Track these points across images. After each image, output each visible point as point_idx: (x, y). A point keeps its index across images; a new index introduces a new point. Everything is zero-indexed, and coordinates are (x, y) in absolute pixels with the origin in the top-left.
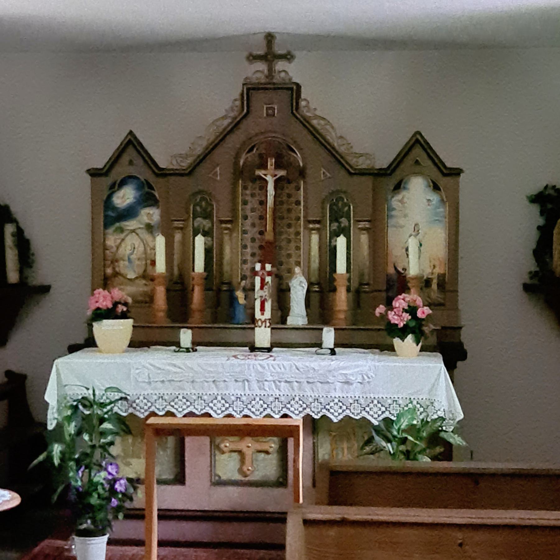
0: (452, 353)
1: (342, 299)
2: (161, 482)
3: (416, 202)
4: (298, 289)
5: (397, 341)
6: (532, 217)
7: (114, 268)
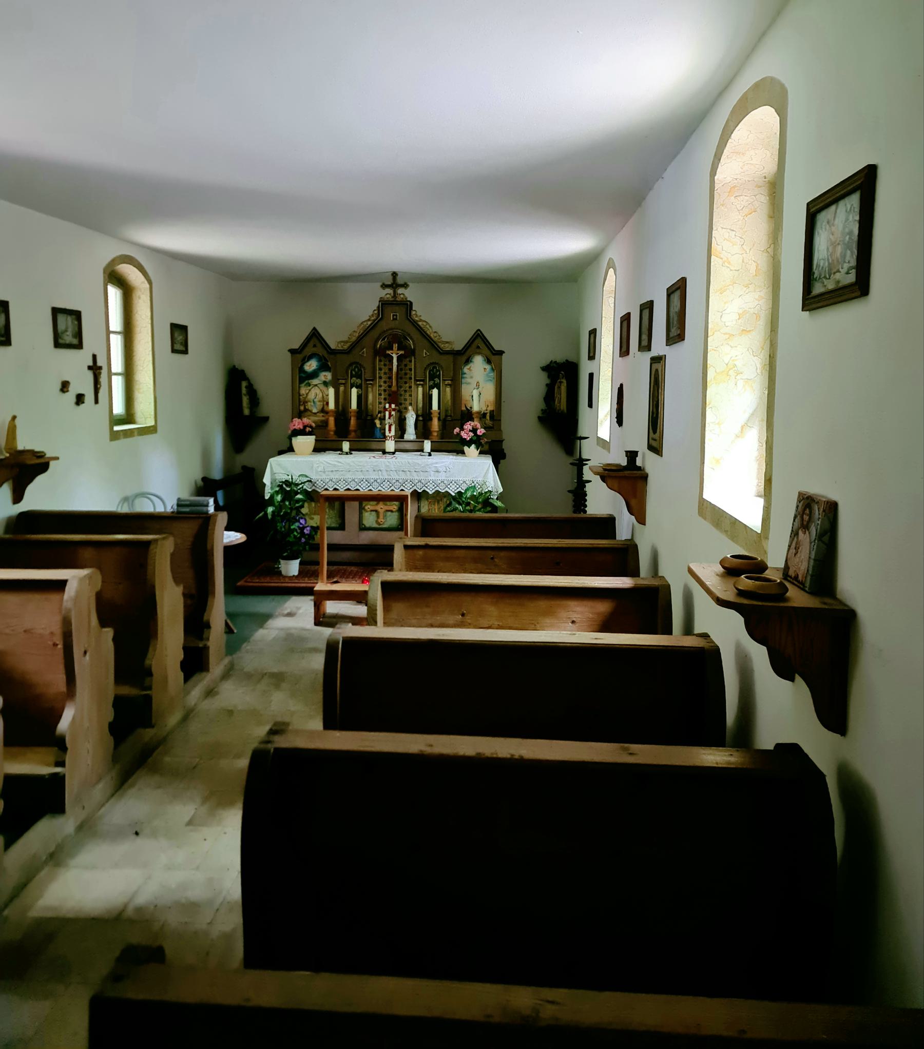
0: (496, 452)
1: (435, 424)
2: (328, 529)
3: (477, 371)
4: (411, 419)
5: (466, 448)
6: (542, 380)
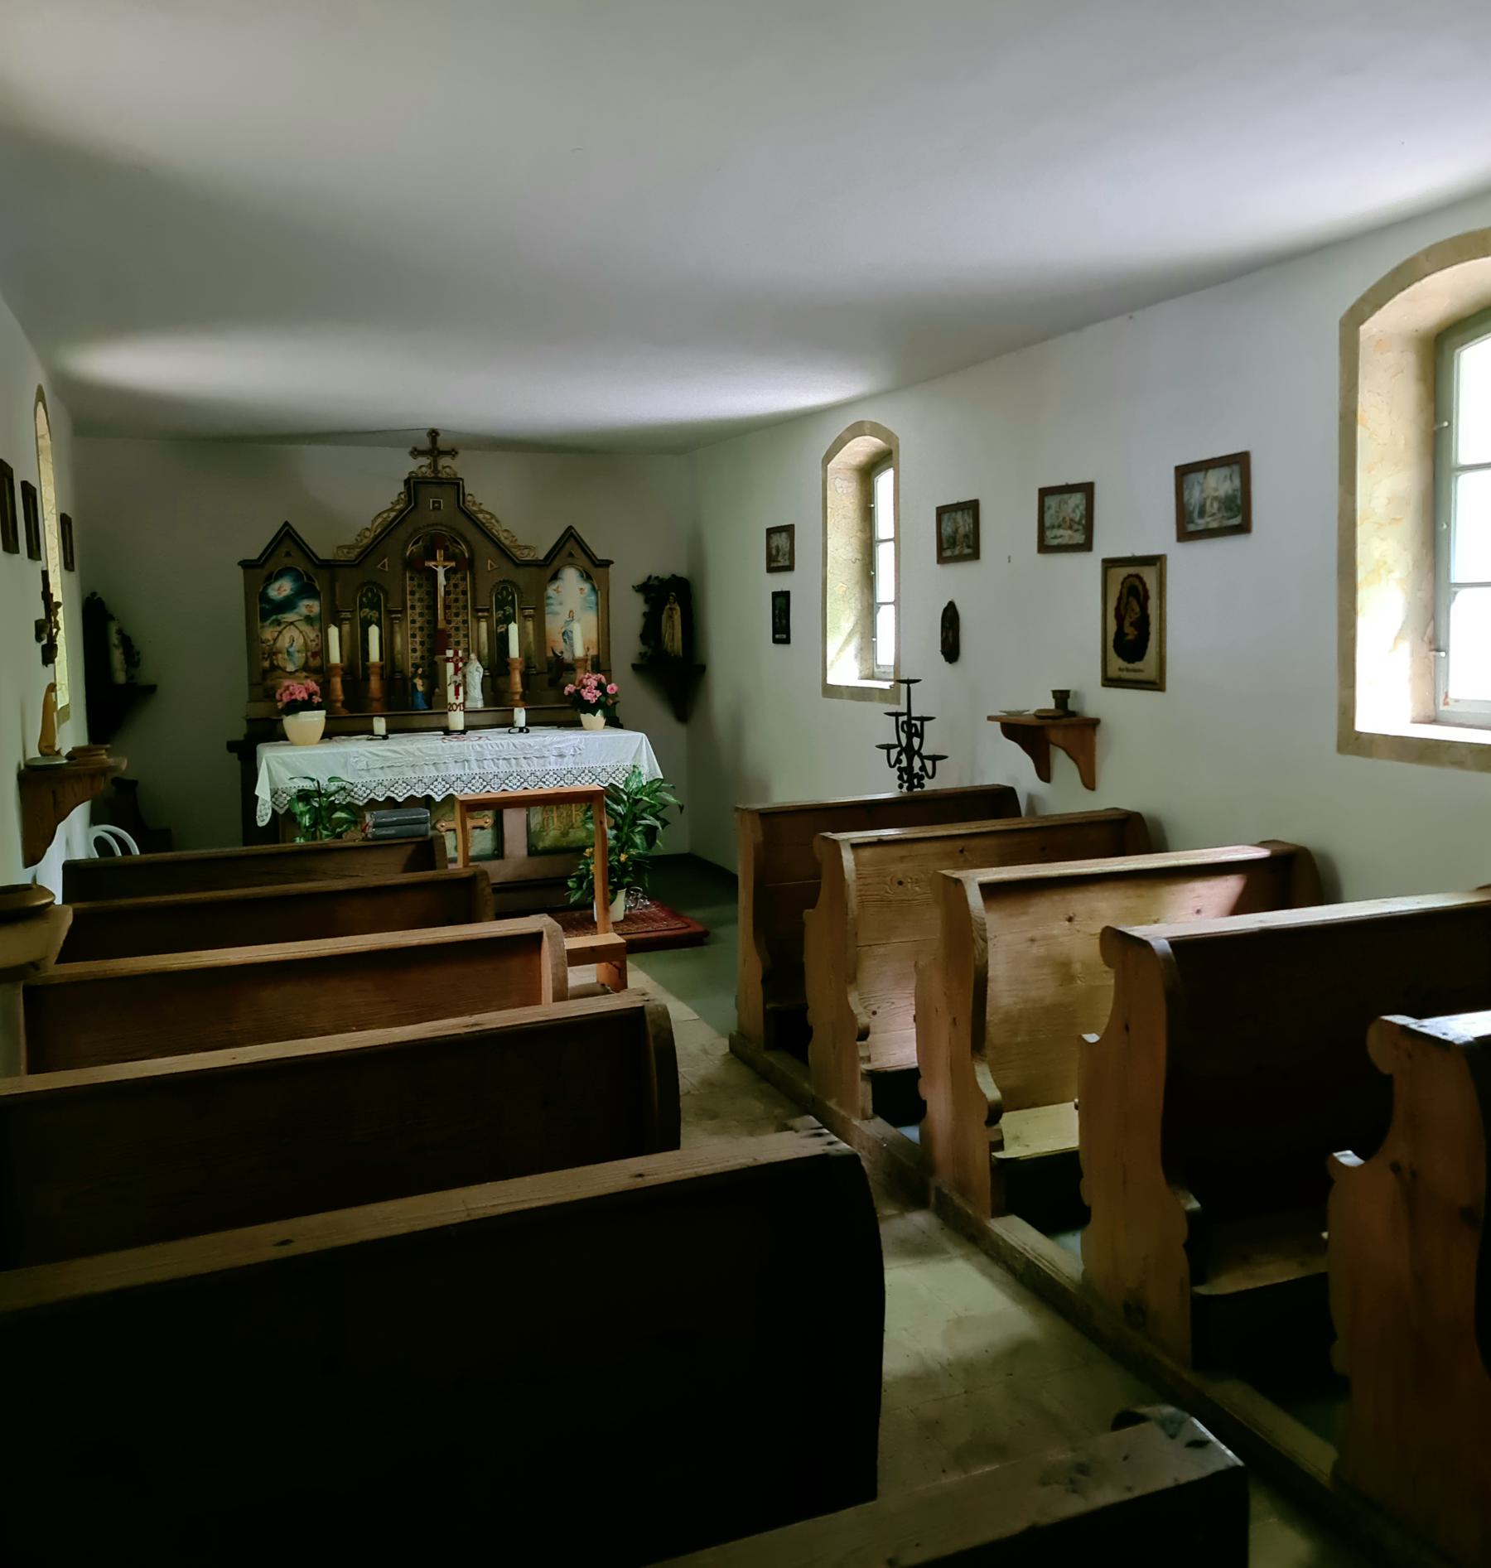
5: (586, 718)
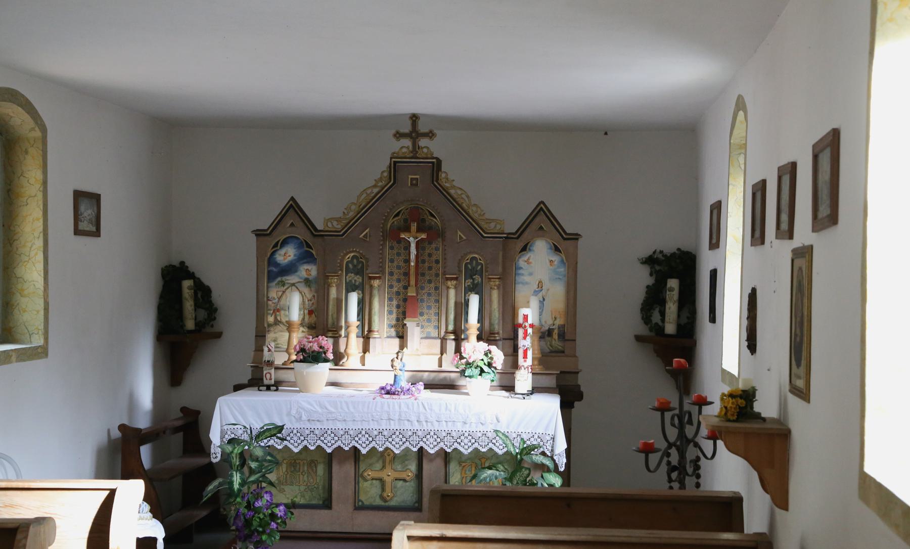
6: (643, 278)
7: (276, 318)
